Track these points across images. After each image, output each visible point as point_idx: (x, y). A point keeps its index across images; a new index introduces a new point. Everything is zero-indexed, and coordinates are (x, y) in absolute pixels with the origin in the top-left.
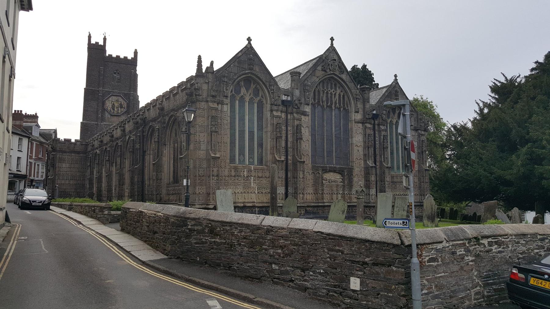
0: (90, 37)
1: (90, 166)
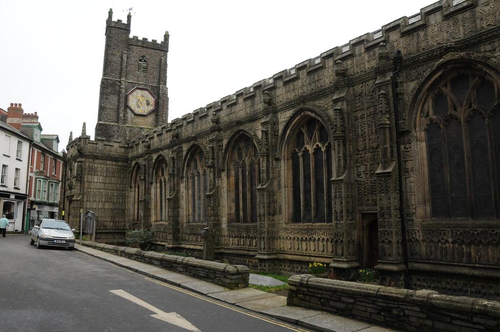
0: (111, 13)
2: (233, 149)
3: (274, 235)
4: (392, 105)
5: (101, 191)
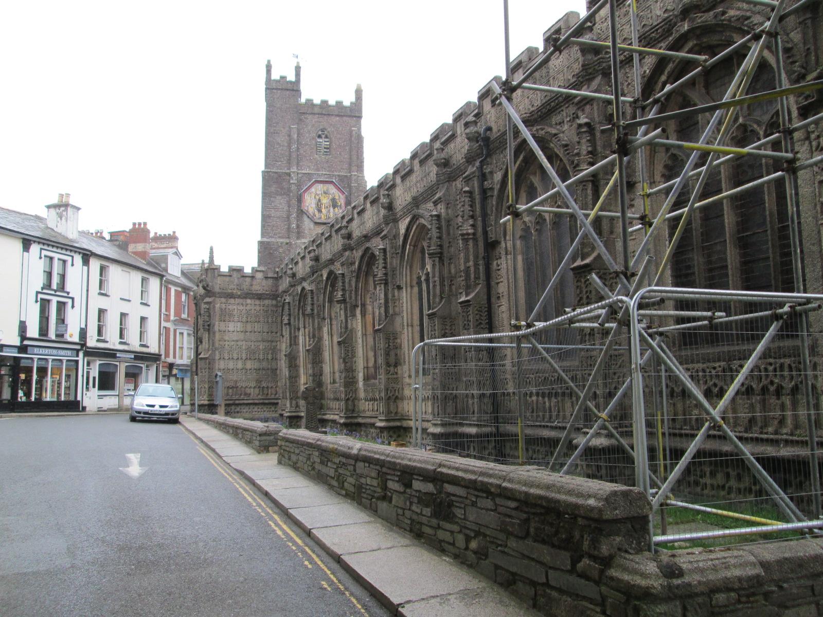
1: (289, 324)
2: (366, 275)
3: (397, 394)
4: (478, 206)
5: (239, 343)
